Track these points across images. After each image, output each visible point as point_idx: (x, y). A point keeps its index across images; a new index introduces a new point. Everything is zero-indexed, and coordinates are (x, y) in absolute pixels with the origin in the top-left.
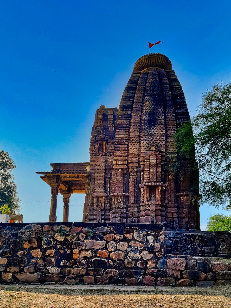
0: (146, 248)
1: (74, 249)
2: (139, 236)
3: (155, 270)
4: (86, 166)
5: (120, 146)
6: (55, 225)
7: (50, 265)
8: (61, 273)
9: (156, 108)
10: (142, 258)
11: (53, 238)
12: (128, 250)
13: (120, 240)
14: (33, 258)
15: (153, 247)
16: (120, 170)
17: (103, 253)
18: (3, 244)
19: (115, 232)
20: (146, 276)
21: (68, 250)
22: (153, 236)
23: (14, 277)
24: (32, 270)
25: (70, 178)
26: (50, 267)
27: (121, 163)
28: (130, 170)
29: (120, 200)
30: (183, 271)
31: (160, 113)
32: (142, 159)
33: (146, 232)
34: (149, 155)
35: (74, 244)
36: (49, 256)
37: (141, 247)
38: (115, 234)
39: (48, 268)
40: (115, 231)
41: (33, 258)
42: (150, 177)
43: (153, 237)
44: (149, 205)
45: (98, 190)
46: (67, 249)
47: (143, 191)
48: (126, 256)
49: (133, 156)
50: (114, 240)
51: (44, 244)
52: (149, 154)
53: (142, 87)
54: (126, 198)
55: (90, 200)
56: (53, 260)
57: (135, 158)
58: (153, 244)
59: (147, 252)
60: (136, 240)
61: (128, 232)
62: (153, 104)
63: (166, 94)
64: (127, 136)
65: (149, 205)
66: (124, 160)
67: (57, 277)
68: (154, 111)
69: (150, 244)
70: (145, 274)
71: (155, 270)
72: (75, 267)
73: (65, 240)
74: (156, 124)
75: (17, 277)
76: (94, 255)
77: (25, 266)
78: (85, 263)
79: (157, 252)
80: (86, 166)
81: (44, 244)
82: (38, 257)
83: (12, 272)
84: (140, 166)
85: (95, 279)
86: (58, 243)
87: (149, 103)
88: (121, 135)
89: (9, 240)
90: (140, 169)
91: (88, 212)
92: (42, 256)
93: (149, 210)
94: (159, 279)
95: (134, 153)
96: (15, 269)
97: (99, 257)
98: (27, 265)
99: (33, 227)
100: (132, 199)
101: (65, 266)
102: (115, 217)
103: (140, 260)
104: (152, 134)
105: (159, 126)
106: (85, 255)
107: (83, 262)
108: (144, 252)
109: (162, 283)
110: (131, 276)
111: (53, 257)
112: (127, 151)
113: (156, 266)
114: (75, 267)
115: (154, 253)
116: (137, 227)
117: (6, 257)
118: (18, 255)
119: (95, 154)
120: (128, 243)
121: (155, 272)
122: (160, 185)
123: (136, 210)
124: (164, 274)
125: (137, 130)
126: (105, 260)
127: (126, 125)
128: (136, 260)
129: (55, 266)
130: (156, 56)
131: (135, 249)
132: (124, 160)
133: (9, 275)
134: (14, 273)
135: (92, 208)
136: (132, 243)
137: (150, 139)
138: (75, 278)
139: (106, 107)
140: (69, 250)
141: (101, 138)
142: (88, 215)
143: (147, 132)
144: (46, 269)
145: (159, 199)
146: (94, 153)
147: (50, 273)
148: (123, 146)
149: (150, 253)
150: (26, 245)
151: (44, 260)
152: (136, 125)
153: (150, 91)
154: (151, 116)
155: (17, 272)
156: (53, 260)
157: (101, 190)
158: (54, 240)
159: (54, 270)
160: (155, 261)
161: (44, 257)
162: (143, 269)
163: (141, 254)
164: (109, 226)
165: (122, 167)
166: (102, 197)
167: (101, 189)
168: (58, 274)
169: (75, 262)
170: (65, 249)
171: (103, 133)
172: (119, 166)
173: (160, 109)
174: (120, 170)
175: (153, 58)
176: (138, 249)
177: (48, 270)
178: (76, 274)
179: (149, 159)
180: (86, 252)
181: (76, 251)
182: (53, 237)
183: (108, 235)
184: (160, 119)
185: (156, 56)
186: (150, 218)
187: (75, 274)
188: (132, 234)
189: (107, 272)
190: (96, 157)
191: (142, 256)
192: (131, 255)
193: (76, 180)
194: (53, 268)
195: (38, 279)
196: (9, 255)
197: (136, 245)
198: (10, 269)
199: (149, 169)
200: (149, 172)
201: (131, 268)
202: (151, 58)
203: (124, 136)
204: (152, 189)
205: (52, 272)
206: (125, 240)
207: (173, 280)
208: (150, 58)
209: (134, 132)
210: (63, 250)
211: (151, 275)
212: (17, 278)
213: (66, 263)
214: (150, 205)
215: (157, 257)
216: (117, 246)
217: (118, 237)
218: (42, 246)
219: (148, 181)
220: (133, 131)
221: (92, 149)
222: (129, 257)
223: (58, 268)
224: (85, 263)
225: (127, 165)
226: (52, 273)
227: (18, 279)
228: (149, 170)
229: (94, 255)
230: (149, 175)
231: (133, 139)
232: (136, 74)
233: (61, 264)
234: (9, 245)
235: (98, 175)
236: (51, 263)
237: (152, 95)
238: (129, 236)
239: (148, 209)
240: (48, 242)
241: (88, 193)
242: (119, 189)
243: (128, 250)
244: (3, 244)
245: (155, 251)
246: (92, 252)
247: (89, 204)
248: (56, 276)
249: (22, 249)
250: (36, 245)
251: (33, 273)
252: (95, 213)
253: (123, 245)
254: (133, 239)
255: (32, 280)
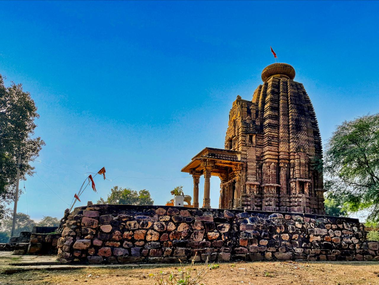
0: (354, 235)
1: (310, 234)
2: (348, 227)
3: (361, 250)
4: (237, 154)
5: (272, 143)
6: (293, 215)
7: (295, 247)
8: (304, 252)
9: (299, 116)
10: (353, 243)
11: (295, 225)
12: (342, 236)
13: (336, 229)
14: (283, 240)
15: (358, 234)
16: (273, 164)
17: (328, 238)
18: (262, 229)
19: (331, 223)
20: (357, 255)
21: (306, 235)
22: (356, 227)
23: (273, 255)
24: (284, 250)
25: (224, 163)
26: (296, 248)
27: (274, 157)
28: (281, 165)
29: (274, 190)
30: (377, 250)
31: (303, 121)
32: (292, 157)
33: (352, 224)
34: (300, 156)
35: (310, 231)
36: (294, 239)
37: (351, 235)
38: (332, 224)
39: (294, 248)
40: (331, 222)
41: (283, 240)
42: (301, 174)
43: (357, 227)
44: (300, 197)
45: (251, 179)
46: (305, 234)
47: (295, 185)
48: (341, 240)
49: (285, 153)
50: (331, 228)
51: (290, 230)
52: (300, 155)
53: (285, 94)
54: (278, 189)
55: (242, 187)
56: (297, 242)
57: (286, 155)
58: (358, 233)
59: (355, 238)
60: (346, 230)
61: (340, 224)
62: (297, 112)
63: (303, 105)
64: (277, 134)
65: (300, 197)
66: (276, 156)
67: (302, 256)
68: (298, 118)
69: (356, 232)
70: (356, 254)
71: (361, 250)
72: (313, 248)
73: (303, 227)
74: (301, 130)
75: (275, 255)
76: (322, 239)
77: (279, 247)
78: (318, 245)
79: (361, 238)
80: (237, 154)
81: (290, 230)
82: (286, 239)
83: (271, 252)
84: (289, 164)
85: (327, 257)
86: (299, 230)
87: (295, 111)
88: (272, 132)
89: (266, 226)
90: (290, 166)
91: (241, 197)
92: (289, 239)
93: (301, 202)
94: (365, 256)
95: (285, 151)
96: (273, 249)
97: (326, 241)
98: (280, 246)
99: (278, 216)
100: (284, 191)
101: (305, 248)
102: (270, 205)
103: (352, 243)
104: (299, 137)
105: (303, 132)
106: (316, 239)
107: (317, 244)
108: (353, 238)
109: (366, 259)
110: (349, 255)
111: (297, 240)
112: (277, 148)
113: (361, 247)
114: (313, 248)
115: (359, 239)
116: (344, 220)
117: (267, 239)
118: (273, 237)
119: (246, 144)
120: (341, 232)
121: (361, 252)
122: (308, 182)
123: (288, 200)
124: (367, 253)
125: (287, 132)
126: (330, 243)
127: (276, 124)
128: (349, 244)
129: (299, 248)
130: (289, 67)
131: (347, 236)
132: (276, 156)
133: (270, 254)
134: (273, 252)
135: (245, 194)
136: (344, 231)
137: (298, 142)
138: (314, 256)
139: (242, 99)
140: (307, 236)
141: (251, 131)
142: (241, 200)
143: (295, 135)
144: (293, 249)
145: (308, 193)
146: (245, 144)
147: (296, 253)
148: (275, 143)
149: (357, 239)
150: (278, 231)
151: (291, 242)
152: (286, 127)
153: (293, 100)
154: (297, 123)
155: (275, 252)
156: (297, 242)
157: (253, 179)
158: (296, 227)
159: (299, 250)
160: (360, 244)
161: (291, 240)
162: (353, 250)
163: (352, 240)
164: (326, 218)
165: (274, 161)
166: (254, 185)
167: (254, 178)
168: (303, 253)
169: (312, 244)
170: (303, 234)
171: (253, 127)
172: (272, 160)
173: (303, 117)
174: (273, 164)
175: (287, 69)
176: (348, 236)
177: (295, 250)
178: (314, 254)
179: (299, 159)
180: (317, 237)
181: (311, 236)
182: (294, 224)
183: (327, 225)
184: (303, 126)
185: (289, 67)
186: (302, 208)
187: (313, 253)
188: (342, 225)
189: (334, 252)
190: (247, 147)
191: (352, 241)
192: (345, 240)
193: (227, 166)
194: (297, 249)
195: (290, 257)
196: (268, 238)
197: (347, 233)
198: (269, 249)
199: (300, 167)
200: (300, 170)
201: (346, 249)
202: (286, 68)
203: (274, 134)
204: (302, 184)
205: (298, 252)
206: (338, 229)
207: (371, 257)
208: (285, 68)
209: (284, 133)
210: (302, 235)
211: (360, 253)
212: (275, 257)
213: (306, 245)
214: (302, 197)
215: (361, 242)
216: (335, 233)
217: (334, 226)
218: (288, 231)
219: (299, 177)
220: (283, 132)
221: (243, 139)
222: (344, 241)
223: (301, 249)
224: (318, 245)
225: (279, 159)
226: (298, 253)
227: (276, 257)
228: (300, 168)
229: (322, 239)
230: (300, 172)
231: (284, 139)
232: (276, 79)
233: (303, 246)
234: (267, 230)
235: (250, 164)
236: (296, 245)
237: (296, 104)
238: (341, 226)
239: (300, 200)
240: (293, 229)
241: (241, 179)
242: (273, 180)
243: (342, 236)
244: (262, 229)
245: (359, 237)
246: (321, 238)
247: (242, 190)
248: (301, 255)
249: (276, 233)
250: (284, 230)
251: (285, 252)
252: (249, 199)
253: (339, 232)
254: (344, 229)
255: (286, 258)
